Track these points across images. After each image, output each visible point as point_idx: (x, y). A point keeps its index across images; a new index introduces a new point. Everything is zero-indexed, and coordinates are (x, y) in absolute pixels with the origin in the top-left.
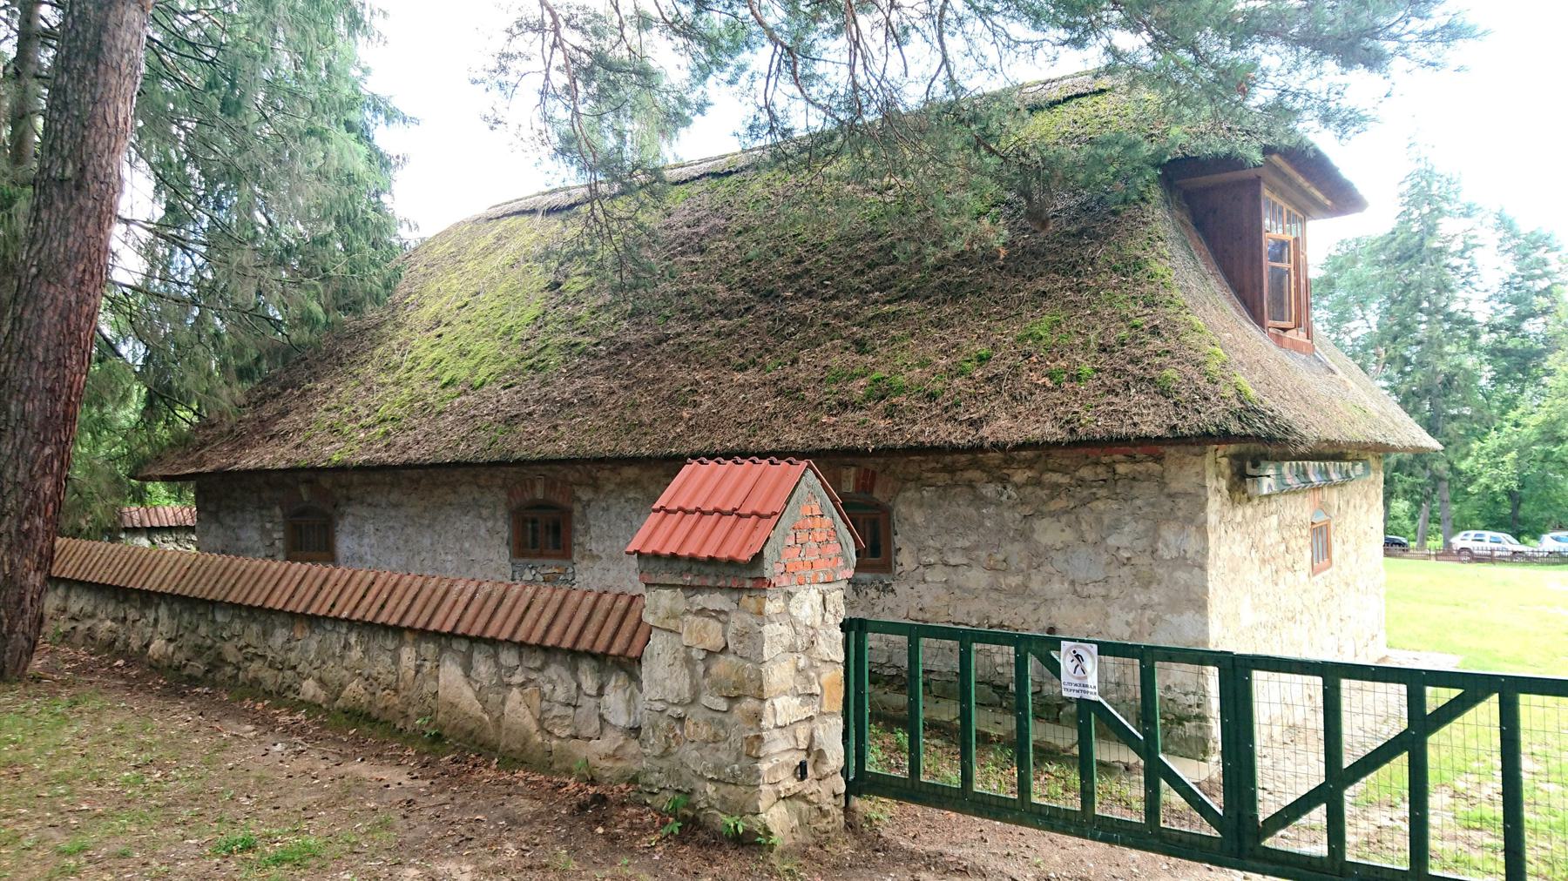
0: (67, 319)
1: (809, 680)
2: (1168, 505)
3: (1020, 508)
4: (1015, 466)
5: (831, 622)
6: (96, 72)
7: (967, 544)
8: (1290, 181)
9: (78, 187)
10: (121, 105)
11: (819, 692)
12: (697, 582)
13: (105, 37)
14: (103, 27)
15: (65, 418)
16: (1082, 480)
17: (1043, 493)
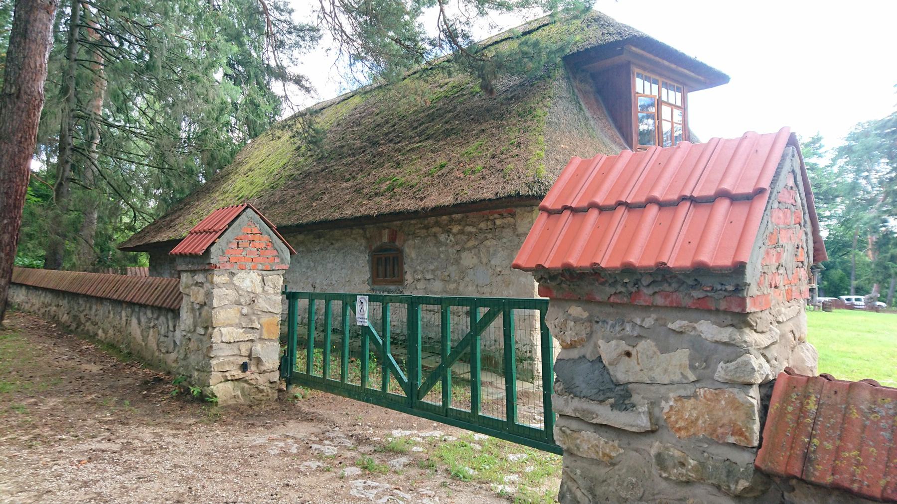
0: (14, 160)
1: (252, 321)
2: (517, 240)
3: (456, 247)
4: (453, 224)
5: (271, 291)
6: (25, 43)
7: (433, 267)
8: (657, 64)
9: (18, 97)
10: (38, 58)
11: (259, 326)
12: (196, 268)
13: (29, 26)
14: (27, 22)
15: (15, 206)
16: (481, 229)
17: (464, 238)
